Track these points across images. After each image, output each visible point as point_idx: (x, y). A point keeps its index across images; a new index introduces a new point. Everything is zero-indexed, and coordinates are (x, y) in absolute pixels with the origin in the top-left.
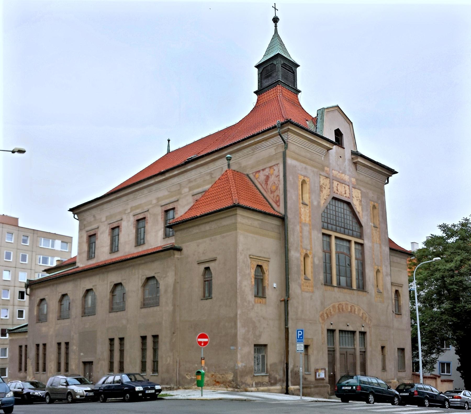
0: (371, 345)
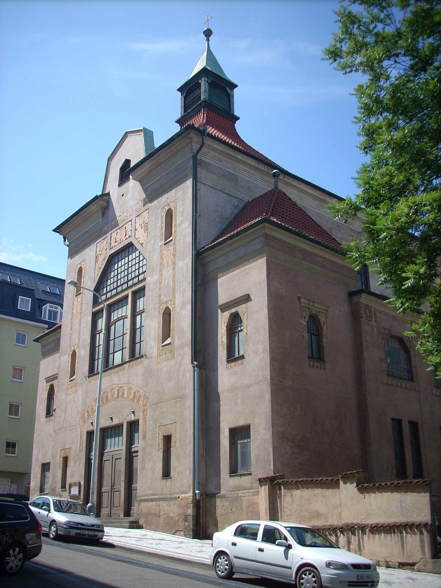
0: (144, 437)
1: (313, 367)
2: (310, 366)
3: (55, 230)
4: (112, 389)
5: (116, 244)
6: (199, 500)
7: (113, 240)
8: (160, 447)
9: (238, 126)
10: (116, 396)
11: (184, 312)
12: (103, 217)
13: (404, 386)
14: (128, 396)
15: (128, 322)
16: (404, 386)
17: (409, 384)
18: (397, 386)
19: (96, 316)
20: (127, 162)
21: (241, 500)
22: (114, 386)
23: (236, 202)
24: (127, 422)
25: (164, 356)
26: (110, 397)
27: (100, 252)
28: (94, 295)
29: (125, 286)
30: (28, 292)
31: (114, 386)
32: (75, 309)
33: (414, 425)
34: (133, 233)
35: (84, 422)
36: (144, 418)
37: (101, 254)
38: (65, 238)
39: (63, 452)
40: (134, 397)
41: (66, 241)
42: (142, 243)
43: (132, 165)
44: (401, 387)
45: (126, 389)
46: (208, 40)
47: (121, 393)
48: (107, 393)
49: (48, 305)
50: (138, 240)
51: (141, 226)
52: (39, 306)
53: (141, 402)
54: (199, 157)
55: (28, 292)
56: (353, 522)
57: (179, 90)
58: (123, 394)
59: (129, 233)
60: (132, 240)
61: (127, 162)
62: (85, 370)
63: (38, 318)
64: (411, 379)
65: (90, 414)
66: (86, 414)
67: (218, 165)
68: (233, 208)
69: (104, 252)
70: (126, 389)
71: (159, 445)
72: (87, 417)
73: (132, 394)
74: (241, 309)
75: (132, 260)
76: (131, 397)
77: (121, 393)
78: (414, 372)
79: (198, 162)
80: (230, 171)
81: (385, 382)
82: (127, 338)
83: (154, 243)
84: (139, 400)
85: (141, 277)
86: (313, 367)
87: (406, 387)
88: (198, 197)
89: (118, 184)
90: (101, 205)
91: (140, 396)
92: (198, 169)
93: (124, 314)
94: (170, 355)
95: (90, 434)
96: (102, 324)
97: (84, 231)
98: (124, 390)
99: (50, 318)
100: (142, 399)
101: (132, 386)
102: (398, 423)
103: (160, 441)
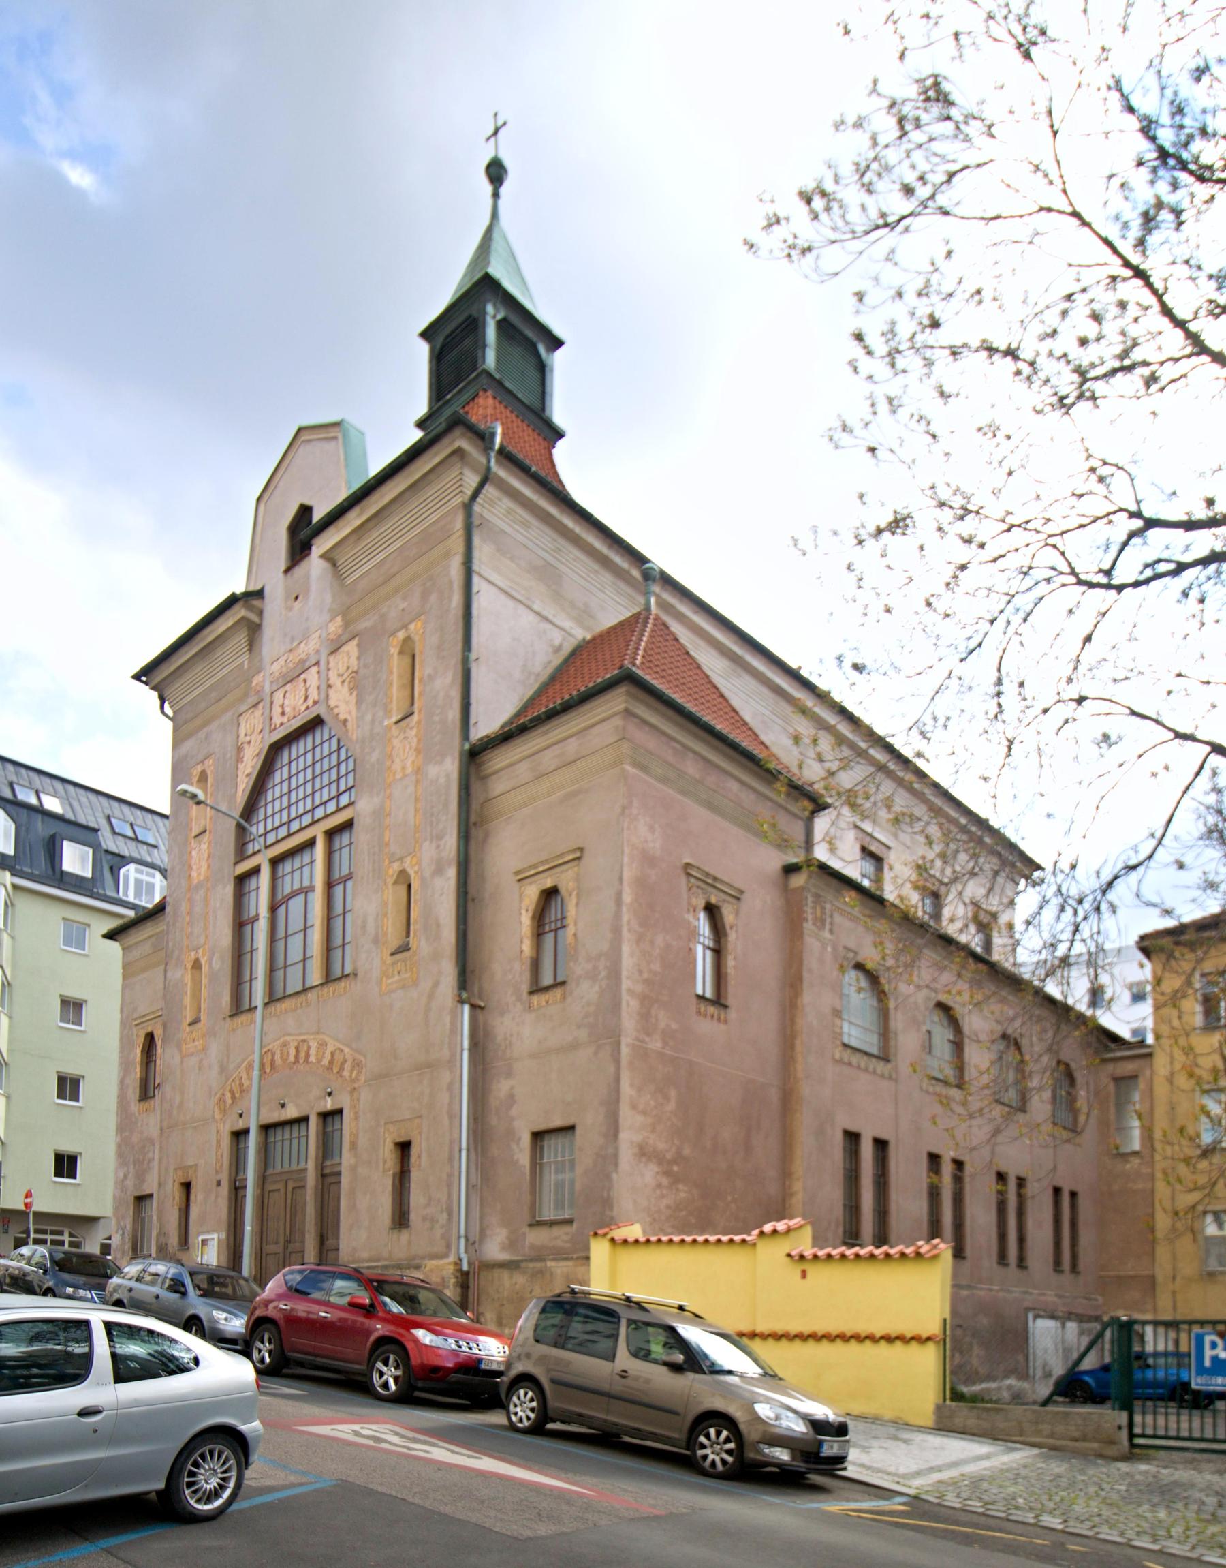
0: (354, 1146)
2: (699, 1013)
3: (137, 677)
4: (285, 1044)
5: (285, 719)
6: (467, 1273)
7: (277, 710)
8: (387, 1166)
9: (561, 453)
10: (292, 1059)
11: (438, 882)
12: (250, 650)
13: (871, 1069)
14: (319, 1061)
15: (317, 900)
16: (871, 1069)
17: (880, 1067)
18: (859, 1067)
20: (305, 511)
21: (552, 1274)
22: (288, 1038)
25: (397, 978)
26: (278, 1061)
27: (248, 738)
28: (239, 826)
29: (307, 820)
30: (85, 833)
31: (288, 1038)
32: (194, 868)
33: (881, 1145)
34: (323, 695)
35: (224, 1111)
36: (353, 1107)
37: (249, 743)
38: (162, 700)
39: (180, 1173)
40: (331, 1062)
41: (166, 705)
42: (345, 721)
43: (317, 516)
44: (866, 1070)
45: (314, 1045)
46: (496, 195)
47: (302, 1055)
48: (273, 1055)
49: (132, 867)
50: (336, 711)
51: (341, 679)
52: (111, 868)
53: (346, 1073)
54: (477, 508)
55: (85, 833)
58: (307, 1055)
59: (314, 695)
60: (321, 710)
61: (305, 511)
62: (224, 1004)
63: (111, 893)
64: (885, 1058)
65: (237, 1095)
66: (228, 1096)
67: (519, 537)
68: (550, 650)
69: (256, 738)
70: (314, 1045)
71: (385, 1162)
72: (229, 1101)
74: (565, 880)
75: (322, 759)
76: (325, 1062)
77: (302, 1055)
78: (892, 1043)
81: (837, 1056)
82: (316, 936)
83: (373, 721)
84: (342, 1069)
85: (344, 800)
86: (705, 1016)
87: (874, 1072)
88: (475, 611)
89: (283, 568)
91: (345, 1061)
92: (476, 541)
93: (306, 883)
94: (408, 975)
95: (240, 1135)
96: (260, 901)
97: (208, 684)
98: (309, 1047)
99: (138, 894)
100: (348, 1066)
101: (327, 1039)
102: (852, 1137)
103: (388, 1154)
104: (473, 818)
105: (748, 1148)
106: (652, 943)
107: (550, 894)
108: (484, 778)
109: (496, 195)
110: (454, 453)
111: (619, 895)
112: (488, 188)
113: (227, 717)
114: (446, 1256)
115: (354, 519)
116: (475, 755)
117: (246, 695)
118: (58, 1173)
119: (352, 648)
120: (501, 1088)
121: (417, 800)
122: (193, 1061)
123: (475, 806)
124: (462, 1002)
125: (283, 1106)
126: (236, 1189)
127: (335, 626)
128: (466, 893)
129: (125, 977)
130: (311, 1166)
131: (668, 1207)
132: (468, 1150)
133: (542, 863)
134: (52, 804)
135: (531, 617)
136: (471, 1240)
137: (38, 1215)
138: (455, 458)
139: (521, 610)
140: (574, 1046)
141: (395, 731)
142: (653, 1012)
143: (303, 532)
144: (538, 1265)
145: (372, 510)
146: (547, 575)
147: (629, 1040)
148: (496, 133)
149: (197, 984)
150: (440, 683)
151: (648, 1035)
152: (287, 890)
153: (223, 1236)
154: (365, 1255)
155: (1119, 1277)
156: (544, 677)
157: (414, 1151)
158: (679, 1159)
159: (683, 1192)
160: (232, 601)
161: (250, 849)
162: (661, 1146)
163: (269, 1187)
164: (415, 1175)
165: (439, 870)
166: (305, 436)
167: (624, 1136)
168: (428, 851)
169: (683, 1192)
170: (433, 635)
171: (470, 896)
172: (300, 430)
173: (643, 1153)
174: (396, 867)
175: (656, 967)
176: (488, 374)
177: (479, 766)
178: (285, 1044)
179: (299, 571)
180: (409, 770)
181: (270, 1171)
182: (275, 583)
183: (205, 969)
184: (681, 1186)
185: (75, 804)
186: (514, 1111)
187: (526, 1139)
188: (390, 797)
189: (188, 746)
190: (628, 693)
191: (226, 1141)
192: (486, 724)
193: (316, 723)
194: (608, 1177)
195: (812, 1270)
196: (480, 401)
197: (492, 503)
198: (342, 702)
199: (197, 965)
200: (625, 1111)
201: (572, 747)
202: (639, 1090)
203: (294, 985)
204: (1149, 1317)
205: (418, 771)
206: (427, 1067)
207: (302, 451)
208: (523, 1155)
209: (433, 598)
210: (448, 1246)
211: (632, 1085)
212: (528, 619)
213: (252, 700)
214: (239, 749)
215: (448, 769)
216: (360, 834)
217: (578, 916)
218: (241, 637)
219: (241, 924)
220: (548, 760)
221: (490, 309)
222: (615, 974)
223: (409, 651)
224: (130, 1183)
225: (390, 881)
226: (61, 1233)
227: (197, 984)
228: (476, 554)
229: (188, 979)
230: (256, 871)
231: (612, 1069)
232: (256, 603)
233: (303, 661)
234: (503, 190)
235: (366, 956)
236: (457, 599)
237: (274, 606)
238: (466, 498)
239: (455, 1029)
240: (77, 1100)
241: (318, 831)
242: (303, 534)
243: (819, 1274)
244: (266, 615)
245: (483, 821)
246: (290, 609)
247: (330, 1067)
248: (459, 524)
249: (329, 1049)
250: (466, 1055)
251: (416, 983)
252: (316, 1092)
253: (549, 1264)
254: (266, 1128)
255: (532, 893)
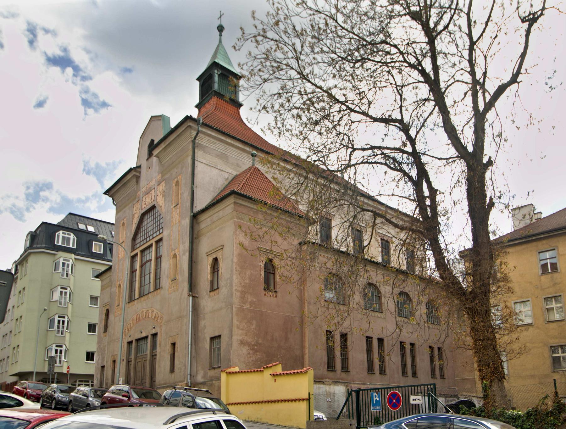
1: (268, 295)
2: (265, 295)
3: (105, 193)
4: (143, 312)
14: (152, 317)
19: (133, 257)
20: (152, 141)
23: (226, 175)
24: (152, 335)
26: (141, 318)
36: (160, 332)
40: (155, 317)
43: (155, 142)
45: (150, 311)
46: (221, 35)
53: (159, 321)
54: (196, 141)
56: (471, 240)
57: (197, 79)
59: (153, 198)
60: (155, 203)
61: (152, 141)
67: (212, 147)
69: (138, 212)
70: (150, 311)
73: (154, 315)
74: (219, 255)
76: (153, 317)
79: (196, 145)
80: (222, 151)
84: (158, 319)
86: (268, 295)
88: (195, 172)
89: (146, 158)
90: (133, 174)
92: (196, 151)
103: (169, 347)
104: (195, 236)
105: (286, 339)
106: (245, 274)
107: (216, 260)
108: (198, 223)
109: (221, 35)
110: (188, 127)
111: (232, 259)
112: (218, 33)
113: (131, 205)
114: (184, 381)
115: (163, 146)
116: (195, 217)
117: (135, 198)
118: (87, 359)
119: (163, 184)
120: (202, 323)
121: (179, 231)
122: (118, 318)
123: (195, 232)
124: (189, 296)
125: (141, 332)
126: (129, 362)
127: (159, 177)
128: (192, 260)
129: (101, 291)
130: (148, 352)
131: (253, 361)
132: (191, 345)
133: (213, 250)
134: (91, 229)
135: (217, 171)
136: (193, 375)
137: (71, 375)
138: (188, 128)
139: (213, 169)
140: (221, 309)
141: (174, 209)
142: (246, 296)
143: (152, 146)
144: (211, 383)
145: (168, 143)
146: (223, 157)
147: (236, 306)
148: (220, 17)
149: (119, 292)
150: (186, 196)
151: (244, 304)
152: (145, 261)
153: (124, 378)
154: (163, 382)
155: (462, 379)
156: (222, 188)
157: (176, 346)
158: (257, 344)
159: (259, 355)
160: (131, 170)
161: (136, 247)
162: (249, 340)
163: (138, 361)
164: (176, 354)
165: (184, 254)
166: (153, 119)
167: (235, 338)
168: (181, 247)
169: (259, 355)
170: (185, 179)
171: (193, 262)
172: (152, 117)
173: (242, 343)
174: (173, 252)
175: (247, 281)
176: (215, 91)
177: (197, 220)
178: (143, 312)
179: (150, 160)
180: (177, 222)
181: (138, 355)
182: (144, 164)
183: (122, 287)
184: (258, 353)
185: (100, 228)
186: (205, 331)
187: (208, 340)
188: (172, 230)
189: (120, 214)
190: (234, 197)
191: (125, 345)
192: (199, 206)
193: (154, 207)
194: (229, 352)
195: (277, 378)
196: (213, 99)
197: (202, 139)
198: (160, 201)
199: (120, 286)
200: (235, 330)
201: (221, 213)
202: (240, 322)
203: (146, 292)
204: (474, 395)
205: (179, 222)
206: (180, 318)
207: (153, 123)
208: (208, 346)
209: (184, 169)
210: (185, 378)
211: (237, 321)
212: (215, 171)
213: (137, 200)
214: (133, 215)
215: (187, 222)
216: (164, 243)
217: (223, 267)
218: (134, 180)
219: (133, 271)
220: (215, 217)
221: (216, 71)
222: (231, 285)
223: (177, 183)
224: (100, 362)
225: (172, 257)
226: (88, 382)
227: (119, 292)
228: (196, 155)
229: (117, 291)
230: (136, 254)
231: (231, 316)
232: (138, 170)
233: (151, 188)
234: (223, 34)
235: (165, 282)
236: (190, 169)
237: (144, 170)
238: (193, 139)
239: (188, 305)
240: (95, 332)
241: (153, 242)
242: (152, 147)
243: (280, 380)
244: (142, 173)
245: (198, 236)
246: (148, 171)
247: (154, 319)
248: (191, 147)
249: (155, 312)
250: (191, 313)
251: (178, 290)
252: (151, 327)
253: (214, 382)
254: (138, 340)
255: (211, 259)
